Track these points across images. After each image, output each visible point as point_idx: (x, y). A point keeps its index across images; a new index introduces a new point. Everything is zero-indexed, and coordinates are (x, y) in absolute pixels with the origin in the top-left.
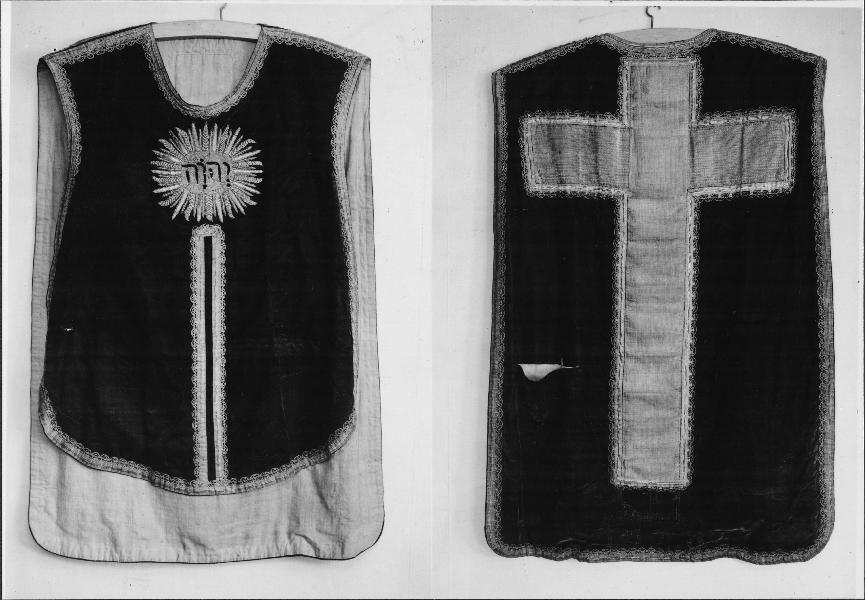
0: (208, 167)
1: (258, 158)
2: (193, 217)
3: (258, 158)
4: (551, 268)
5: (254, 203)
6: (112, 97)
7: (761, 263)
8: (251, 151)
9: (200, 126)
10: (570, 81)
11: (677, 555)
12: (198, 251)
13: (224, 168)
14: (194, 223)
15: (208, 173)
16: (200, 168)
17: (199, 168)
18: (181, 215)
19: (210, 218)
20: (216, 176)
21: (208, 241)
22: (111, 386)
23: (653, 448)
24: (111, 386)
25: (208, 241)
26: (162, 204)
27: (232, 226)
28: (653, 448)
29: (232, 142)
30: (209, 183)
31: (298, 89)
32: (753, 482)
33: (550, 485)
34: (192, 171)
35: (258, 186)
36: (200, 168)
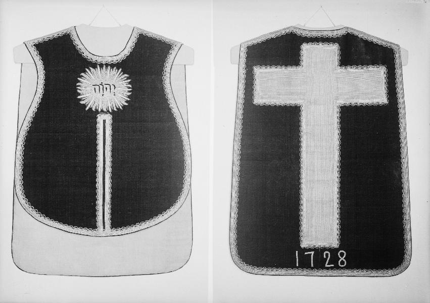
0: (105, 86)
1: (130, 83)
2: (97, 110)
3: (130, 83)
4: (270, 137)
5: (127, 104)
6: (61, 58)
7: (371, 139)
8: (127, 79)
9: (108, 111)
10: (283, 50)
11: (396, 174)
12: (100, 126)
13: (112, 87)
14: (97, 112)
15: (105, 89)
16: (101, 87)
17: (101, 87)
18: (90, 109)
19: (105, 110)
20: (108, 90)
21: (104, 121)
22: (57, 179)
23: (320, 223)
24: (57, 179)
25: (104, 121)
26: (82, 102)
27: (118, 115)
28: (320, 223)
29: (117, 75)
30: (105, 93)
31: (147, 60)
32: (374, 236)
33: (268, 235)
34: (97, 88)
35: (129, 97)
36: (101, 87)
